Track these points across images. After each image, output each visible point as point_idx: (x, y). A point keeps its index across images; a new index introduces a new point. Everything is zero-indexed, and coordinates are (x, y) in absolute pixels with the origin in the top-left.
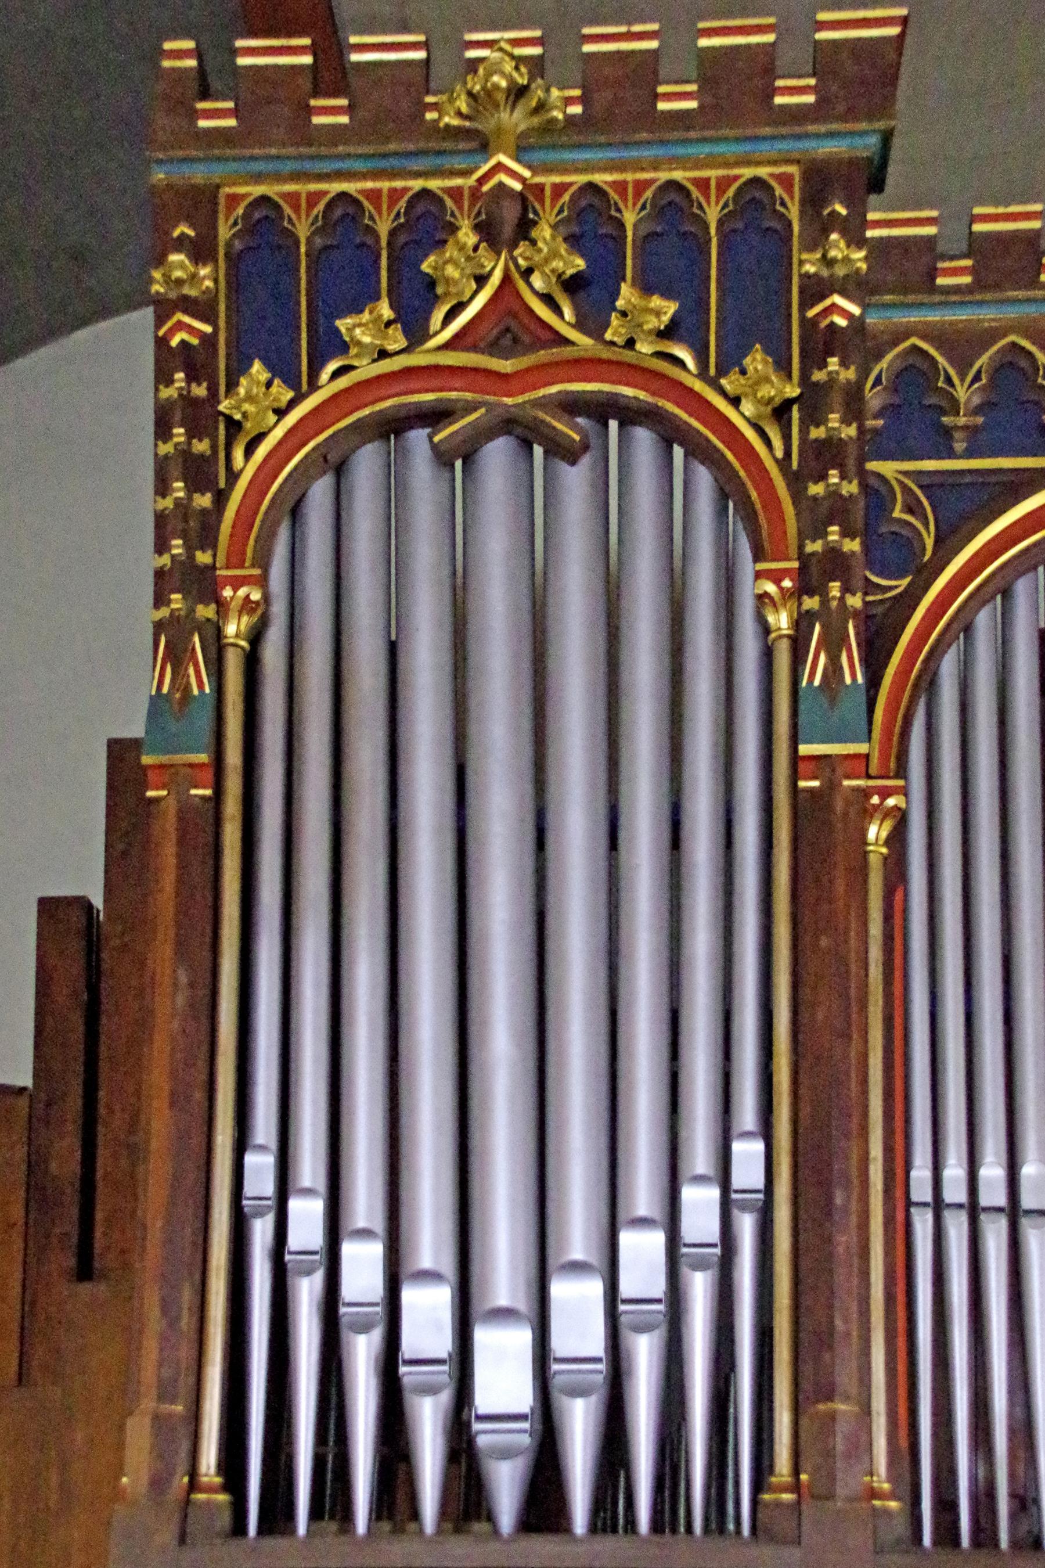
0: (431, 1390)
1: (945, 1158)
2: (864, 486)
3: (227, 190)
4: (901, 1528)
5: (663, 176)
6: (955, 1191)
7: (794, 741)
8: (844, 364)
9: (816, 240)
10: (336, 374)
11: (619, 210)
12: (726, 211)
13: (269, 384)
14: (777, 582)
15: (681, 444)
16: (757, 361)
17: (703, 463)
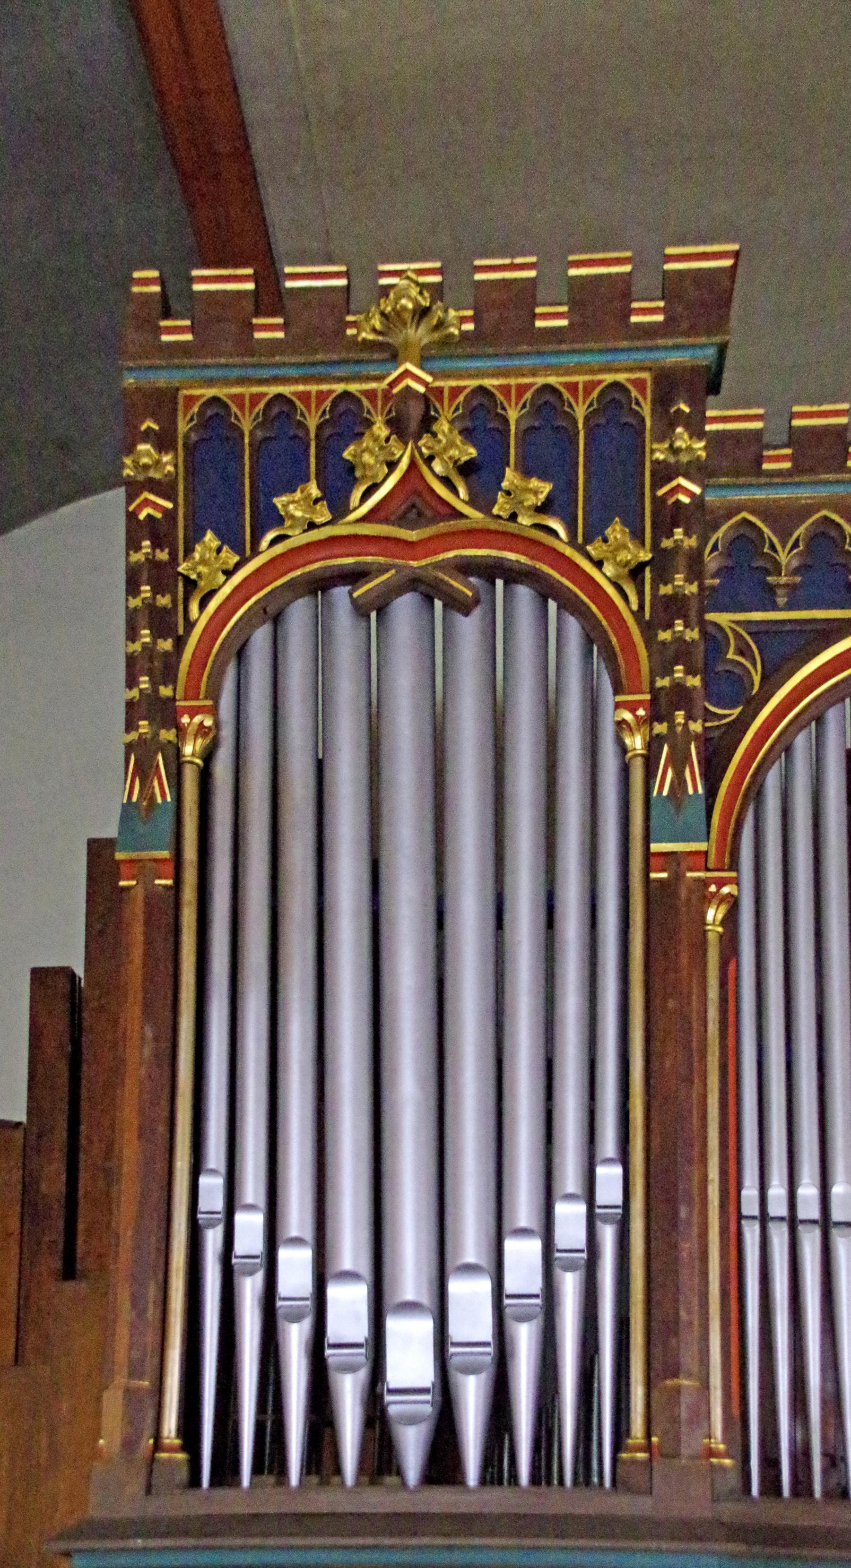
0: (351, 1368)
1: (769, 1180)
2: (704, 633)
3: (185, 392)
4: (734, 1481)
5: (540, 381)
6: (778, 1207)
7: (647, 840)
8: (687, 534)
9: (665, 433)
10: (274, 542)
11: (504, 409)
12: (591, 409)
13: (219, 550)
14: (633, 711)
15: (554, 599)
16: (616, 531)
17: (572, 615)
